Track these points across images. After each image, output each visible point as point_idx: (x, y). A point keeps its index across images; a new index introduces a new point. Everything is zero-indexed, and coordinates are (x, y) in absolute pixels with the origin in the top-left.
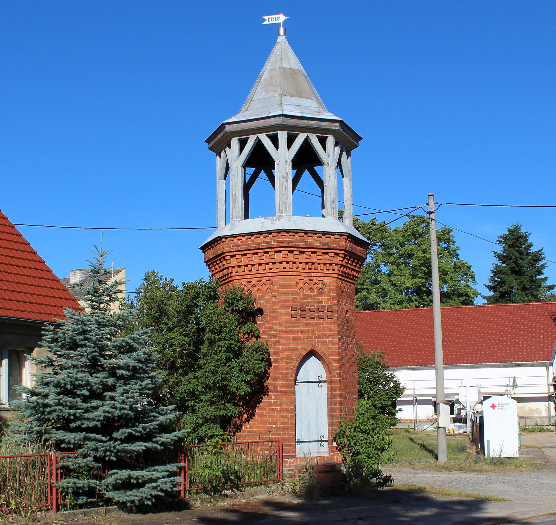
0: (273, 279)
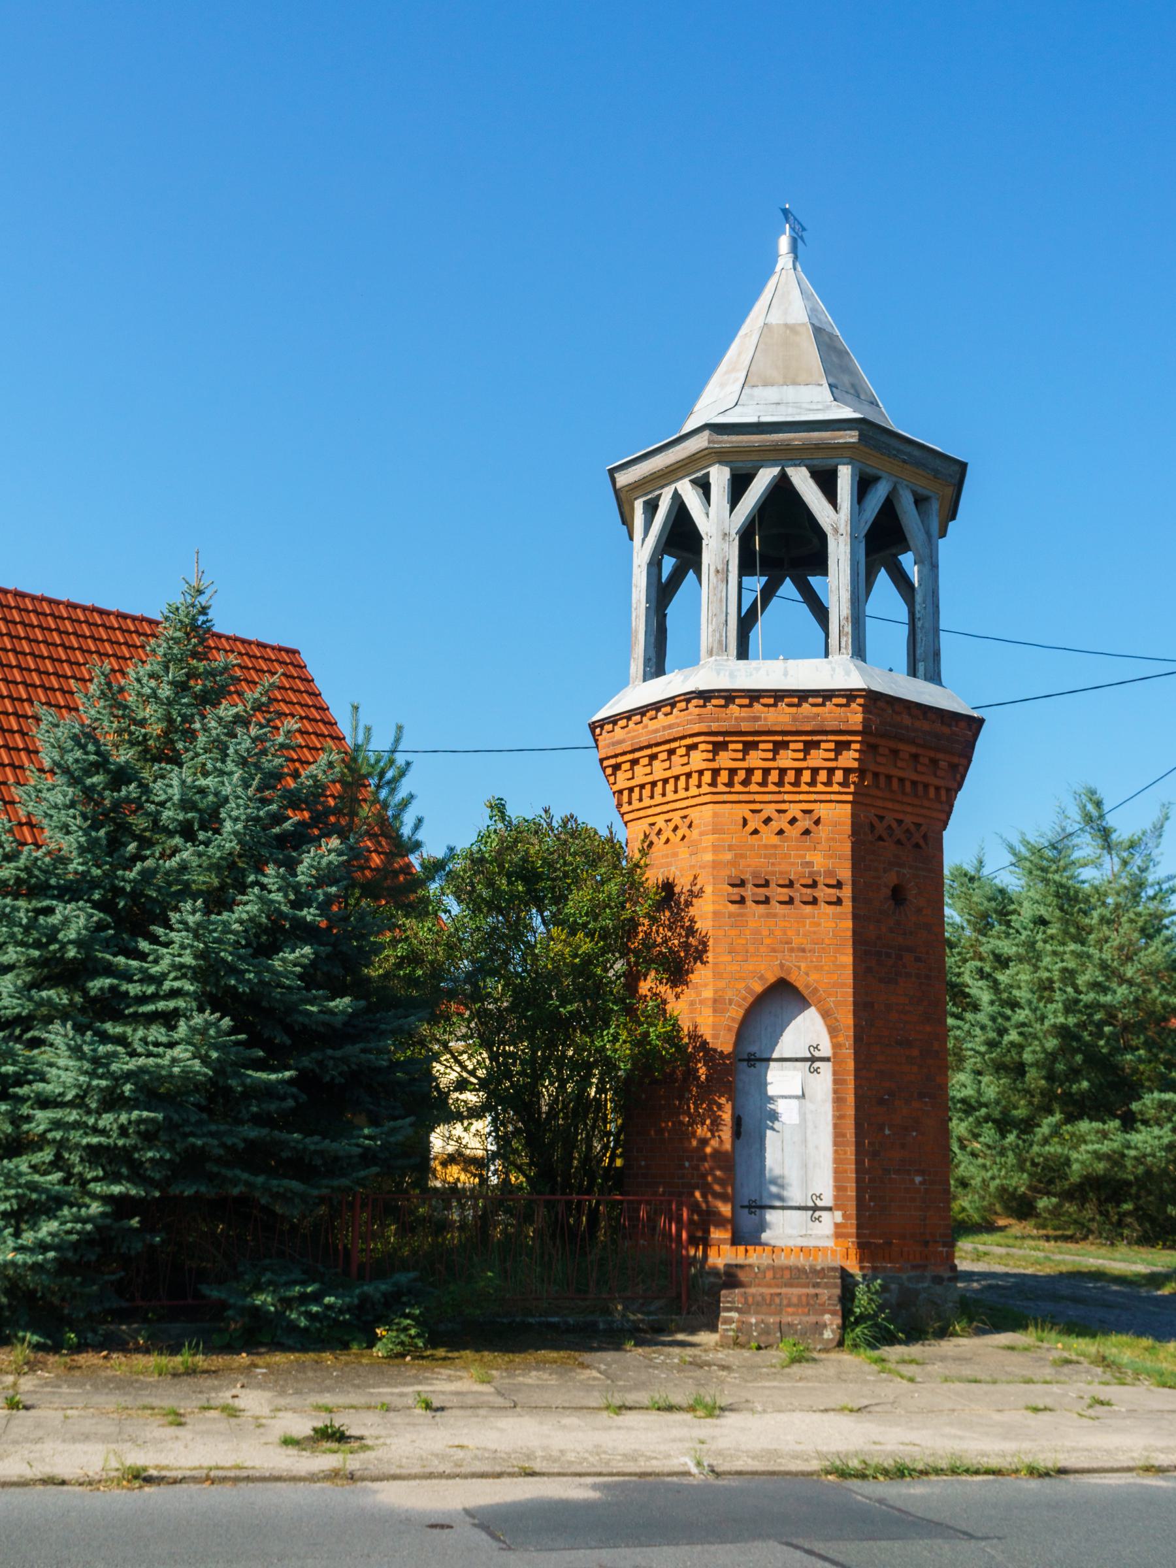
0: (693, 814)
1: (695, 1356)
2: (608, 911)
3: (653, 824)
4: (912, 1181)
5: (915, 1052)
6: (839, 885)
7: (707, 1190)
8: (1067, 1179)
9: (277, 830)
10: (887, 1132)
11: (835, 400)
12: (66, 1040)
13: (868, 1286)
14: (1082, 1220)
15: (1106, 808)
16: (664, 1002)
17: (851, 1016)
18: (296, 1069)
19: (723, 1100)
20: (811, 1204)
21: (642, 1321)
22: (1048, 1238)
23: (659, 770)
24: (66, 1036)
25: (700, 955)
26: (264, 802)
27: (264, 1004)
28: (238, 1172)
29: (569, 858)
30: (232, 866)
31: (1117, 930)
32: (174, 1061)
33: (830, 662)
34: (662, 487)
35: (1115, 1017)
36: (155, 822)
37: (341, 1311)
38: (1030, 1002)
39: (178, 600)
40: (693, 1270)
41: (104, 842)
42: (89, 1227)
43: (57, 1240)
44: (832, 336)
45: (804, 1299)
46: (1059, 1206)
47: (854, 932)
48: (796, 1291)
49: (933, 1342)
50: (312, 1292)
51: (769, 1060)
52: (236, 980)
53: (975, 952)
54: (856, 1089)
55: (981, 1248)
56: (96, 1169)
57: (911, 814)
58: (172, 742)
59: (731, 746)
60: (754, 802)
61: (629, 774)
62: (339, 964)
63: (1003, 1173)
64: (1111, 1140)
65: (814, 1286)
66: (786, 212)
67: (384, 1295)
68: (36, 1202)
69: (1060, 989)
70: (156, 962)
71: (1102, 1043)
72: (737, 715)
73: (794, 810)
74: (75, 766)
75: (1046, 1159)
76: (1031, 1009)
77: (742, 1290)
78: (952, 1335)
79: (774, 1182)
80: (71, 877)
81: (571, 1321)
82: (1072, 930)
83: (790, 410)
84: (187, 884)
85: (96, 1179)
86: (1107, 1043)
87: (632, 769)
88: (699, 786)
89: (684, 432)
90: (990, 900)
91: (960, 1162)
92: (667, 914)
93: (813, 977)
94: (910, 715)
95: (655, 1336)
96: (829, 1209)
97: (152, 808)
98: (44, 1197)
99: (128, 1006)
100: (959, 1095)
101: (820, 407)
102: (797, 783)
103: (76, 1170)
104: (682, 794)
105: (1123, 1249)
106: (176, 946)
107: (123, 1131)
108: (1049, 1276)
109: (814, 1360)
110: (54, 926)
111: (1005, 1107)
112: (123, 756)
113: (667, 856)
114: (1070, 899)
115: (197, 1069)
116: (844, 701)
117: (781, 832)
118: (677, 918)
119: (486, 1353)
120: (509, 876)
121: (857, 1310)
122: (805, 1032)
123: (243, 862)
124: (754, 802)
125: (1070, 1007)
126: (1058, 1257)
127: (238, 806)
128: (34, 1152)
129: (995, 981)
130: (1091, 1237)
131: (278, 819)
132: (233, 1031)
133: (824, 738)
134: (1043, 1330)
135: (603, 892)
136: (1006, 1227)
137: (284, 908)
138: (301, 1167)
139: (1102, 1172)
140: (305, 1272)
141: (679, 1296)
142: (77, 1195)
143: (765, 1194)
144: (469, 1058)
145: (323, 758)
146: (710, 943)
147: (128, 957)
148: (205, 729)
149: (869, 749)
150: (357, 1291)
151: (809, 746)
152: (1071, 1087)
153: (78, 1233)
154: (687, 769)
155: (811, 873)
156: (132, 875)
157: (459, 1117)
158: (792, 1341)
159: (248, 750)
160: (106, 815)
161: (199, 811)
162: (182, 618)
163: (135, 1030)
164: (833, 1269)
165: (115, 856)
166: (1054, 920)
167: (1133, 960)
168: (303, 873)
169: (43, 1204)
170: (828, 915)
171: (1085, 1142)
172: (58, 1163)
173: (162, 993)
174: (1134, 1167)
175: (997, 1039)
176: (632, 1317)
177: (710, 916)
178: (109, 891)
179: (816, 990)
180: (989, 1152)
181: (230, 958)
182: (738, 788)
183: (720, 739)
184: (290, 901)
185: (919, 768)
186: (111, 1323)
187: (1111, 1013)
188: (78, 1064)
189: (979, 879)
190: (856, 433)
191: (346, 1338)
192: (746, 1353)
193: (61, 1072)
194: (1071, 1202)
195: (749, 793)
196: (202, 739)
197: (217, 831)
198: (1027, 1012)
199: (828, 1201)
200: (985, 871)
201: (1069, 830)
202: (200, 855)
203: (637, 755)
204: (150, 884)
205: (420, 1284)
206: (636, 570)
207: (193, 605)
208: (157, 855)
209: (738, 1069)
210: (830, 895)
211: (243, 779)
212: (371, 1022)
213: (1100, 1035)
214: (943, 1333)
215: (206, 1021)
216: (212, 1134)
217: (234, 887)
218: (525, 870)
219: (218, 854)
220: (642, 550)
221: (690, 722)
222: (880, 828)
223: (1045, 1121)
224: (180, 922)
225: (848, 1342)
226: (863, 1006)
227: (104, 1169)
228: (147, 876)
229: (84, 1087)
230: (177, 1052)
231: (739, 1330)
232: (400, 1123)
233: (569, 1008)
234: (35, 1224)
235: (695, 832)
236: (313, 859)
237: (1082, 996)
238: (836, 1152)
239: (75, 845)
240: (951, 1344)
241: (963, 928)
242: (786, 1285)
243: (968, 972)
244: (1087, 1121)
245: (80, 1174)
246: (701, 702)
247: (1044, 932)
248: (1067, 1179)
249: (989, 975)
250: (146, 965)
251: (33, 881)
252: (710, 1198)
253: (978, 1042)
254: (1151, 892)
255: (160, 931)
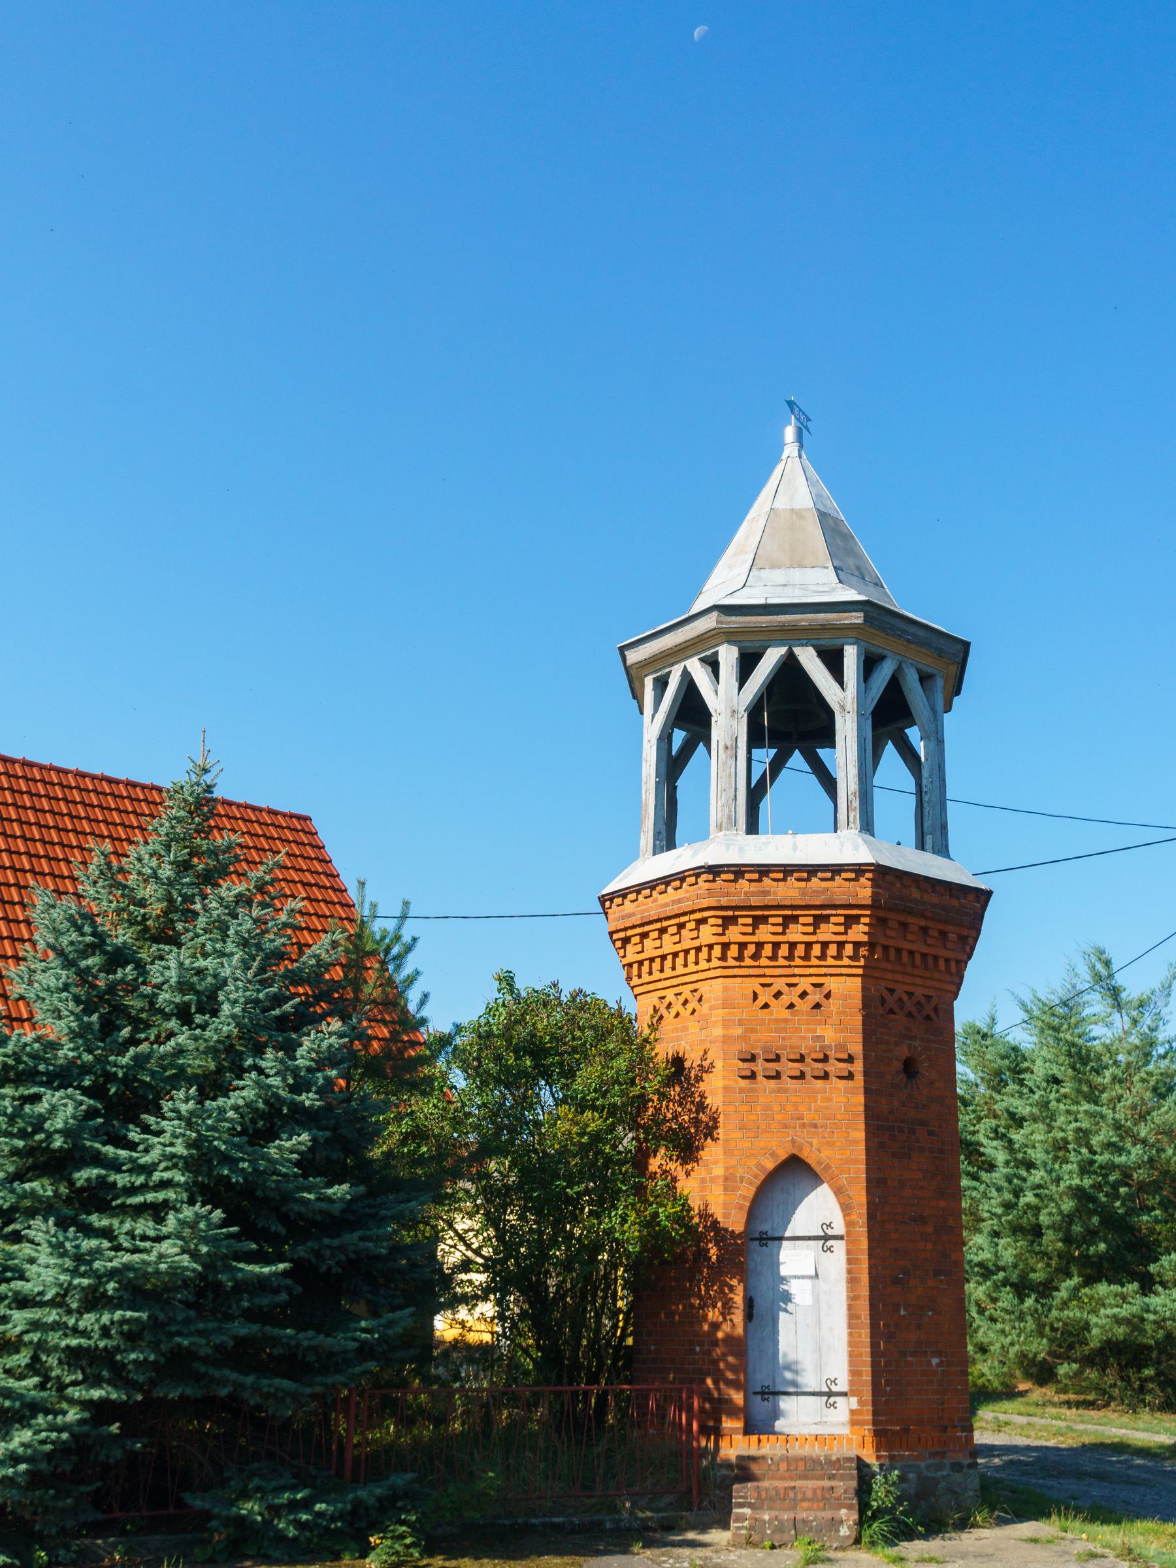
0: (703, 988)
1: (706, 1558)
2: (617, 1088)
3: (664, 998)
4: (929, 1363)
5: (930, 1229)
6: (850, 1059)
7: (718, 1378)
8: (1087, 1344)
9: (277, 1012)
10: (902, 1313)
11: (840, 582)
12: (47, 1237)
13: (885, 1477)
14: (1103, 1386)
15: (1115, 967)
16: (674, 1180)
17: (864, 1193)
18: (291, 1261)
19: (734, 1282)
20: (825, 1389)
21: (651, 1518)
22: (1069, 1404)
23: (669, 944)
24: (47, 1232)
25: (710, 1131)
26: (265, 983)
27: (259, 1193)
28: (227, 1372)
29: (578, 1034)
30: (230, 1049)
31: (1129, 1089)
32: (161, 1256)
33: (839, 837)
34: (672, 665)
35: (1130, 1177)
36: (152, 1004)
37: (333, 1519)
38: (1045, 1164)
39: (183, 779)
40: (704, 1462)
41: (97, 1027)
42: (65, 1436)
43: (29, 1451)
44: (837, 521)
45: (819, 1492)
46: (1078, 1374)
47: (866, 1106)
48: (811, 1484)
49: (953, 1534)
50: (302, 1498)
51: (781, 1239)
52: (230, 1169)
53: (989, 1110)
54: (870, 1268)
55: (1002, 1417)
56: (75, 1373)
57: (922, 986)
58: (172, 922)
59: (741, 921)
60: (764, 976)
61: (639, 948)
62: (341, 1139)
63: (1022, 1339)
64: (1130, 1303)
65: (829, 1478)
66: (791, 404)
67: (379, 1499)
68: (9, 1409)
69: (1075, 1150)
70: (146, 1151)
71: (1118, 1204)
72: (746, 889)
73: (805, 984)
74: (70, 949)
75: (1066, 1324)
76: (1046, 1171)
77: (755, 1484)
78: (973, 1526)
79: (788, 1367)
80: (61, 1061)
81: (576, 1520)
82: (1085, 1088)
83: (797, 592)
84: (182, 1069)
85: (75, 1383)
86: (1123, 1204)
87: (641, 942)
88: (709, 960)
89: (692, 612)
90: (1003, 1057)
91: (979, 1327)
92: (678, 1089)
93: (825, 1154)
94: (918, 888)
95: (665, 1535)
96: (845, 1394)
97: (148, 990)
98: (17, 1404)
99: (115, 1198)
100: (976, 1259)
101: (826, 589)
102: (806, 957)
103: (53, 1374)
104: (692, 967)
105: (1145, 1415)
106: (168, 1135)
107: (105, 1332)
108: (1071, 1449)
109: (829, 1560)
110: (40, 1115)
111: (1023, 1270)
112: (123, 936)
113: (677, 1030)
114: (1081, 1058)
115: (186, 1264)
116: (853, 875)
117: (791, 1006)
118: (687, 1093)
119: (486, 1561)
120: (516, 1052)
121: (875, 1504)
122: (818, 1209)
123: (241, 1045)
124: (764, 976)
125: (1085, 1168)
126: (1081, 1427)
127: (237, 989)
128: (10, 1354)
129: (1010, 1141)
130: (1112, 1404)
131: (278, 1000)
132: (225, 1223)
133: (834, 912)
134: (1067, 1519)
135: (612, 1068)
136: (1027, 1391)
137: (281, 1092)
138: (294, 1365)
139: (1122, 1337)
140: (295, 1476)
141: (690, 1491)
142: (54, 1400)
143: (778, 1379)
144: (476, 1236)
145: (326, 939)
146: (721, 1119)
147: (117, 1147)
148: (206, 909)
149: (879, 922)
150: (351, 1496)
151: (819, 920)
152: (1088, 1249)
153: (53, 1443)
154: (696, 943)
155: (821, 1047)
156: (125, 1060)
157: (465, 1299)
158: (807, 1539)
159: (249, 931)
160: (101, 998)
161: (197, 993)
162: (186, 796)
163: (122, 1222)
164: (849, 1459)
165: (108, 1040)
166: (1066, 1079)
167: (1146, 1120)
168: (302, 1057)
169: (17, 1412)
170: (839, 1089)
171: (1104, 1305)
172: (36, 1366)
173: (151, 1184)
174: (1154, 1331)
175: (1013, 1200)
176: (640, 1515)
177: (720, 1091)
178: (101, 1076)
179: (828, 1167)
180: (1007, 1317)
181: (224, 1147)
182: (748, 962)
183: (730, 913)
184: (288, 1085)
185: (929, 941)
186: (86, 1536)
187: (1126, 1174)
188: (59, 1261)
189: (992, 1036)
190: (862, 615)
191: (337, 1547)
192: (760, 1554)
193: (41, 1270)
194: (1092, 1368)
195: (759, 967)
196: (202, 921)
197: (215, 1013)
198: (1042, 1173)
199: (842, 1386)
200: (998, 1028)
201: (1080, 987)
202: (196, 1039)
203: (647, 928)
204: (144, 1069)
205: (417, 1485)
206: (645, 745)
207: (198, 784)
208: (152, 1038)
209: (746, 1252)
210: (841, 1069)
211: (243, 961)
212: (370, 1207)
213: (1117, 1196)
214: (964, 1524)
215: (196, 1214)
216: (200, 1333)
217: (231, 1071)
218: (533, 1044)
219: (215, 1038)
220: (652, 726)
221: (698, 897)
222: (891, 1001)
223: (1063, 1284)
224: (173, 1111)
225: (865, 1539)
226: (876, 1183)
227: (83, 1373)
228: (140, 1061)
229: (65, 1285)
230: (167, 1247)
231: (751, 1528)
232: (398, 1314)
233: (576, 1189)
234: (7, 1434)
235: (705, 1008)
236: (313, 1042)
237: (1097, 1157)
238: (850, 1334)
239: (66, 1031)
240: (973, 1536)
241: (977, 1085)
242: (800, 1478)
243: (982, 1131)
244: (1105, 1284)
245: (58, 1378)
246: (711, 877)
247: (1057, 1091)
248: (1087, 1344)
249: (1004, 1135)
250: (135, 1155)
251: (21, 1067)
252: (722, 1386)
253: (991, 1205)
254: (1161, 1051)
255: (151, 1120)
